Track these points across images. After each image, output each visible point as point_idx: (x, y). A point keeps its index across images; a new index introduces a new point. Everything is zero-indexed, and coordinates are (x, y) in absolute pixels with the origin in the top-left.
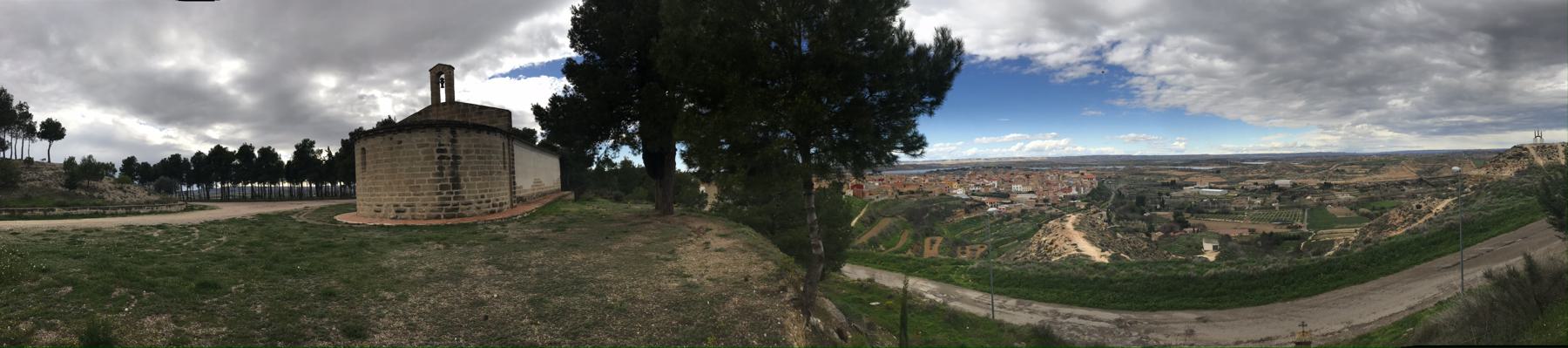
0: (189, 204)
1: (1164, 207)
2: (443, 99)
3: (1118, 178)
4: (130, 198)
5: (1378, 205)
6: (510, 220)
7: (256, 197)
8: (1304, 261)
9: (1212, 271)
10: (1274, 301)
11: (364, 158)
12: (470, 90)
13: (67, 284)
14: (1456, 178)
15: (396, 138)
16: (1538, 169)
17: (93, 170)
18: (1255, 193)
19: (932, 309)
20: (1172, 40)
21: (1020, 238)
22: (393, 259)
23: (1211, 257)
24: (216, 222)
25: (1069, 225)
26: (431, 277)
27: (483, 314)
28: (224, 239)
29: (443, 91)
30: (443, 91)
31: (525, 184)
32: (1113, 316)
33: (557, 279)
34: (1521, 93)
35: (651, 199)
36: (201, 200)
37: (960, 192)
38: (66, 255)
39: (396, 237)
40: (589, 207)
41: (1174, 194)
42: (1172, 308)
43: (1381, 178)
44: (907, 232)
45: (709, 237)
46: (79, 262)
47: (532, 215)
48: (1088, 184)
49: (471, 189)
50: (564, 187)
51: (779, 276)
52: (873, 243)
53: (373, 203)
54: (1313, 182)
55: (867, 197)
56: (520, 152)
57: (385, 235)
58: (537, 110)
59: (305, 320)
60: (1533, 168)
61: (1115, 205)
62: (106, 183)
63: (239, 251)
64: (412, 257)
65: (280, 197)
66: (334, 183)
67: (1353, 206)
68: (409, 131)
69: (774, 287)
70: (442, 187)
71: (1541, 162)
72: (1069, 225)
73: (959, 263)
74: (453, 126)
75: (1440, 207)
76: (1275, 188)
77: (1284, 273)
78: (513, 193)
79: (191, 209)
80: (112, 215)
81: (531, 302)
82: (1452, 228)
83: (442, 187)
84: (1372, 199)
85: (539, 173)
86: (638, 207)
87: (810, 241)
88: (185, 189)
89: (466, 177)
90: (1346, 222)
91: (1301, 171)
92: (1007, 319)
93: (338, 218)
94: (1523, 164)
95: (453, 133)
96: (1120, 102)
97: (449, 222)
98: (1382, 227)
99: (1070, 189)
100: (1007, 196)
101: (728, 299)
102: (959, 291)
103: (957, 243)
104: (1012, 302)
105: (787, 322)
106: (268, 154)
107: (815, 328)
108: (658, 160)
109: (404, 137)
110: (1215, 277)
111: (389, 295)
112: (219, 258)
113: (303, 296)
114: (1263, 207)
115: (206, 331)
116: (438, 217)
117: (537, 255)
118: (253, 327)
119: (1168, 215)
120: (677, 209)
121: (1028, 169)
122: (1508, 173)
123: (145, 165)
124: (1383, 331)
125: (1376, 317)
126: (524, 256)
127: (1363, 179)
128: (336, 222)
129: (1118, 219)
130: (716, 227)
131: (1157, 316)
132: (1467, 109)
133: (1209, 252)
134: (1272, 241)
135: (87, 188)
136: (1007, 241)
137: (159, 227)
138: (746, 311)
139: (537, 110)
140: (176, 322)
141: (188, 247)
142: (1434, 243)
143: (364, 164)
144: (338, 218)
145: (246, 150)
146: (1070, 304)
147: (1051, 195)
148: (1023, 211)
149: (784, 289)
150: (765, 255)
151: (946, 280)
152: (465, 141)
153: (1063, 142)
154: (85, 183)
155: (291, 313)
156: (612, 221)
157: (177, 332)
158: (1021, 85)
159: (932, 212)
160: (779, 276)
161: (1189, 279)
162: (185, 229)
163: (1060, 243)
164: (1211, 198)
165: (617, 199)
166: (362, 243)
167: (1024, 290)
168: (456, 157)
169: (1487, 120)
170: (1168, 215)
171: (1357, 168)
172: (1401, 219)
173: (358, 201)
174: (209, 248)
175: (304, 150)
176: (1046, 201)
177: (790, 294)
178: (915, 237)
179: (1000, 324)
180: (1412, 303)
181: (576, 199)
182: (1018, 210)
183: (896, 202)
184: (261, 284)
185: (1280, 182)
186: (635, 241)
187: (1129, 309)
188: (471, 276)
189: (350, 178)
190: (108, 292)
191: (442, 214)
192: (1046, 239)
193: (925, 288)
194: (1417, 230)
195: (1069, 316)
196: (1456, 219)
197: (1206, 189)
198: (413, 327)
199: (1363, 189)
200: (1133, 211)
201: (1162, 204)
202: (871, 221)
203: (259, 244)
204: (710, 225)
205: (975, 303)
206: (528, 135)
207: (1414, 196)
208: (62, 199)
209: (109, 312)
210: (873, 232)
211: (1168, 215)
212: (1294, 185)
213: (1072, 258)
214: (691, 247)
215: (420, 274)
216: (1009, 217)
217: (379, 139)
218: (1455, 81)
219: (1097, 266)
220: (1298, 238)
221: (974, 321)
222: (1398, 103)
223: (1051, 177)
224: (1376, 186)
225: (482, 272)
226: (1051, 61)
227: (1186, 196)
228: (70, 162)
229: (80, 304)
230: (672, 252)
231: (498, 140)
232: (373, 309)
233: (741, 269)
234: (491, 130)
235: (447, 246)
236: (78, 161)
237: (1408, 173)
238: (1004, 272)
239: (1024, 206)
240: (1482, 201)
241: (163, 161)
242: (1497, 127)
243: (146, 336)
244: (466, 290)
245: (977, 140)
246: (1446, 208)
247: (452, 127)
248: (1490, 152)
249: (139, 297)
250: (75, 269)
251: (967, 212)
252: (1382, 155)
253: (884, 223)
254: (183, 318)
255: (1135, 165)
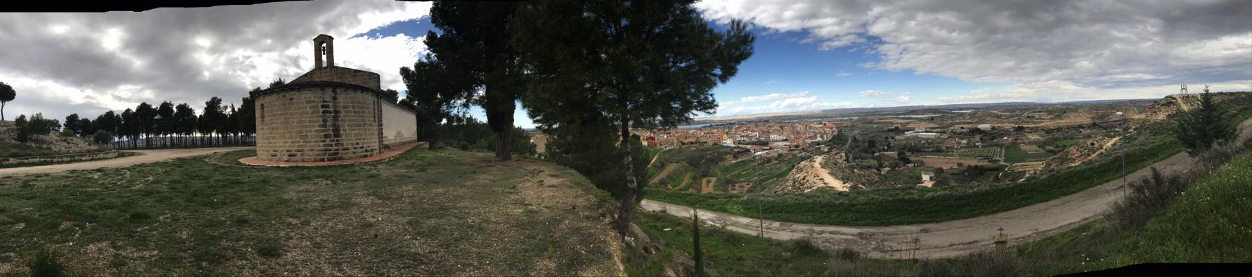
0: (121, 152)
1: (890, 148)
2: (325, 65)
3: (853, 127)
4: (73, 149)
5: (1060, 143)
6: (380, 162)
7: (174, 145)
8: (1002, 185)
9: (930, 194)
10: (979, 215)
11: (263, 112)
12: (348, 55)
13: (20, 221)
14: (1125, 120)
15: (288, 95)
16: (1184, 112)
17: (40, 126)
18: (961, 135)
19: (713, 232)
20: (920, 17)
21: (778, 176)
22: (292, 192)
23: (930, 185)
24: (143, 165)
25: (817, 165)
26: (325, 207)
27: (373, 233)
28: (151, 178)
29: (324, 58)
30: (324, 58)
31: (390, 135)
32: (855, 231)
33: (425, 206)
34: (1177, 58)
35: (491, 148)
36: (129, 148)
37: (729, 142)
38: (19, 197)
39: (291, 176)
40: (441, 154)
41: (897, 137)
42: (901, 223)
43: (1063, 122)
44: (689, 175)
45: (541, 177)
46: (31, 202)
47: (397, 159)
48: (830, 132)
49: (349, 137)
50: (419, 139)
51: (599, 206)
52: (663, 183)
53: (270, 147)
54: (1008, 126)
55: (658, 147)
56: (387, 109)
57: (318, 172)
58: (405, 71)
59: (224, 243)
60: (1180, 113)
61: (852, 147)
62: (52, 136)
63: (164, 188)
64: (308, 191)
65: (194, 145)
66: (236, 134)
67: (1041, 145)
68: (299, 90)
69: (595, 214)
70: (326, 136)
71: (1185, 108)
72: (817, 165)
73: (732, 197)
74: (335, 86)
75: (1110, 143)
76: (978, 131)
77: (986, 194)
78: (381, 142)
79: (123, 155)
80: (59, 163)
81: (410, 223)
82: (1118, 159)
83: (326, 136)
84: (1056, 139)
85: (400, 126)
86: (481, 155)
87: (614, 175)
88: (116, 139)
89: (345, 129)
90: (1036, 157)
91: (999, 117)
92: (774, 237)
93: (241, 161)
94: (1174, 109)
95: (334, 91)
96: (869, 65)
97: (333, 163)
98: (1063, 160)
99: (815, 137)
100: (766, 144)
101: (560, 221)
102: (734, 219)
103: (728, 182)
104: (776, 224)
105: (608, 239)
106: (184, 109)
107: (628, 245)
108: (500, 117)
109: (295, 94)
110: (933, 198)
111: (294, 221)
112: (148, 194)
113: (221, 224)
114: (968, 146)
115: (140, 254)
116: (323, 160)
117: (407, 189)
118: (180, 250)
119: (893, 154)
120: (514, 156)
121: (782, 122)
122: (1161, 116)
123: (86, 121)
124: (1063, 235)
125: (1059, 225)
126: (398, 190)
127: (1048, 123)
128: (240, 164)
129: (854, 158)
130: (548, 170)
131: (889, 230)
132: (1137, 69)
133: (927, 180)
134: (978, 172)
135: (36, 141)
136: (768, 179)
137: (98, 170)
138: (575, 231)
139: (405, 71)
140: (114, 247)
141: (121, 186)
142: (1104, 171)
143: (263, 117)
144: (241, 161)
145: (166, 107)
146: (822, 223)
147: (801, 142)
148: (780, 155)
149: (604, 215)
150: (587, 191)
151: (722, 210)
152: (343, 98)
153: (812, 99)
154: (35, 136)
155: (213, 238)
156: (462, 164)
157: (116, 256)
158: (798, 50)
159: (704, 159)
160: (599, 206)
161: (912, 201)
162: (118, 171)
163: (811, 179)
164: (927, 140)
165: (464, 148)
166: (263, 181)
167: (785, 215)
168: (336, 112)
169: (1151, 77)
170: (893, 154)
171: (1044, 115)
172: (1078, 154)
173: (258, 148)
174: (139, 186)
175: (213, 105)
176: (797, 146)
177: (608, 219)
178: (695, 178)
179: (769, 240)
180: (1087, 216)
181: (431, 148)
182: (775, 155)
183: (680, 151)
184: (186, 214)
185: (982, 126)
186: (483, 179)
187: (868, 225)
188: (358, 205)
189: (250, 128)
190: (56, 226)
191: (326, 157)
192: (800, 176)
193: (707, 217)
194: (1091, 162)
195: (823, 232)
196: (1121, 153)
197: (923, 133)
198: (318, 246)
199: (1049, 131)
200: (866, 151)
201: (889, 146)
202: (661, 166)
203: (180, 182)
204: (542, 168)
205: (746, 226)
206: (392, 95)
207: (1089, 137)
208: (15, 151)
209: (57, 242)
210: (663, 174)
211: (893, 154)
212: (993, 128)
213: (821, 190)
214: (528, 184)
215: (316, 204)
216: (769, 161)
217: (274, 97)
218: (1132, 48)
219: (840, 193)
220: (997, 169)
221: (748, 240)
222: (1085, 64)
223: (799, 128)
224: (1059, 129)
225: (367, 201)
226: (824, 32)
227: (907, 139)
228: (21, 120)
229: (32, 237)
230: (514, 187)
231: (370, 99)
232: (282, 234)
233: (570, 200)
234: (363, 89)
235: (334, 182)
236: (28, 119)
237: (1085, 119)
238: (769, 202)
239: (780, 151)
240: (1141, 138)
241: (100, 118)
242: (1158, 82)
243: (89, 260)
244: (355, 216)
245: (744, 99)
246: (1114, 145)
247: (334, 86)
248: (1149, 101)
249: (82, 227)
250: (27, 208)
251: (735, 157)
252: (1064, 104)
253: (671, 168)
254: (120, 243)
255: (867, 116)
